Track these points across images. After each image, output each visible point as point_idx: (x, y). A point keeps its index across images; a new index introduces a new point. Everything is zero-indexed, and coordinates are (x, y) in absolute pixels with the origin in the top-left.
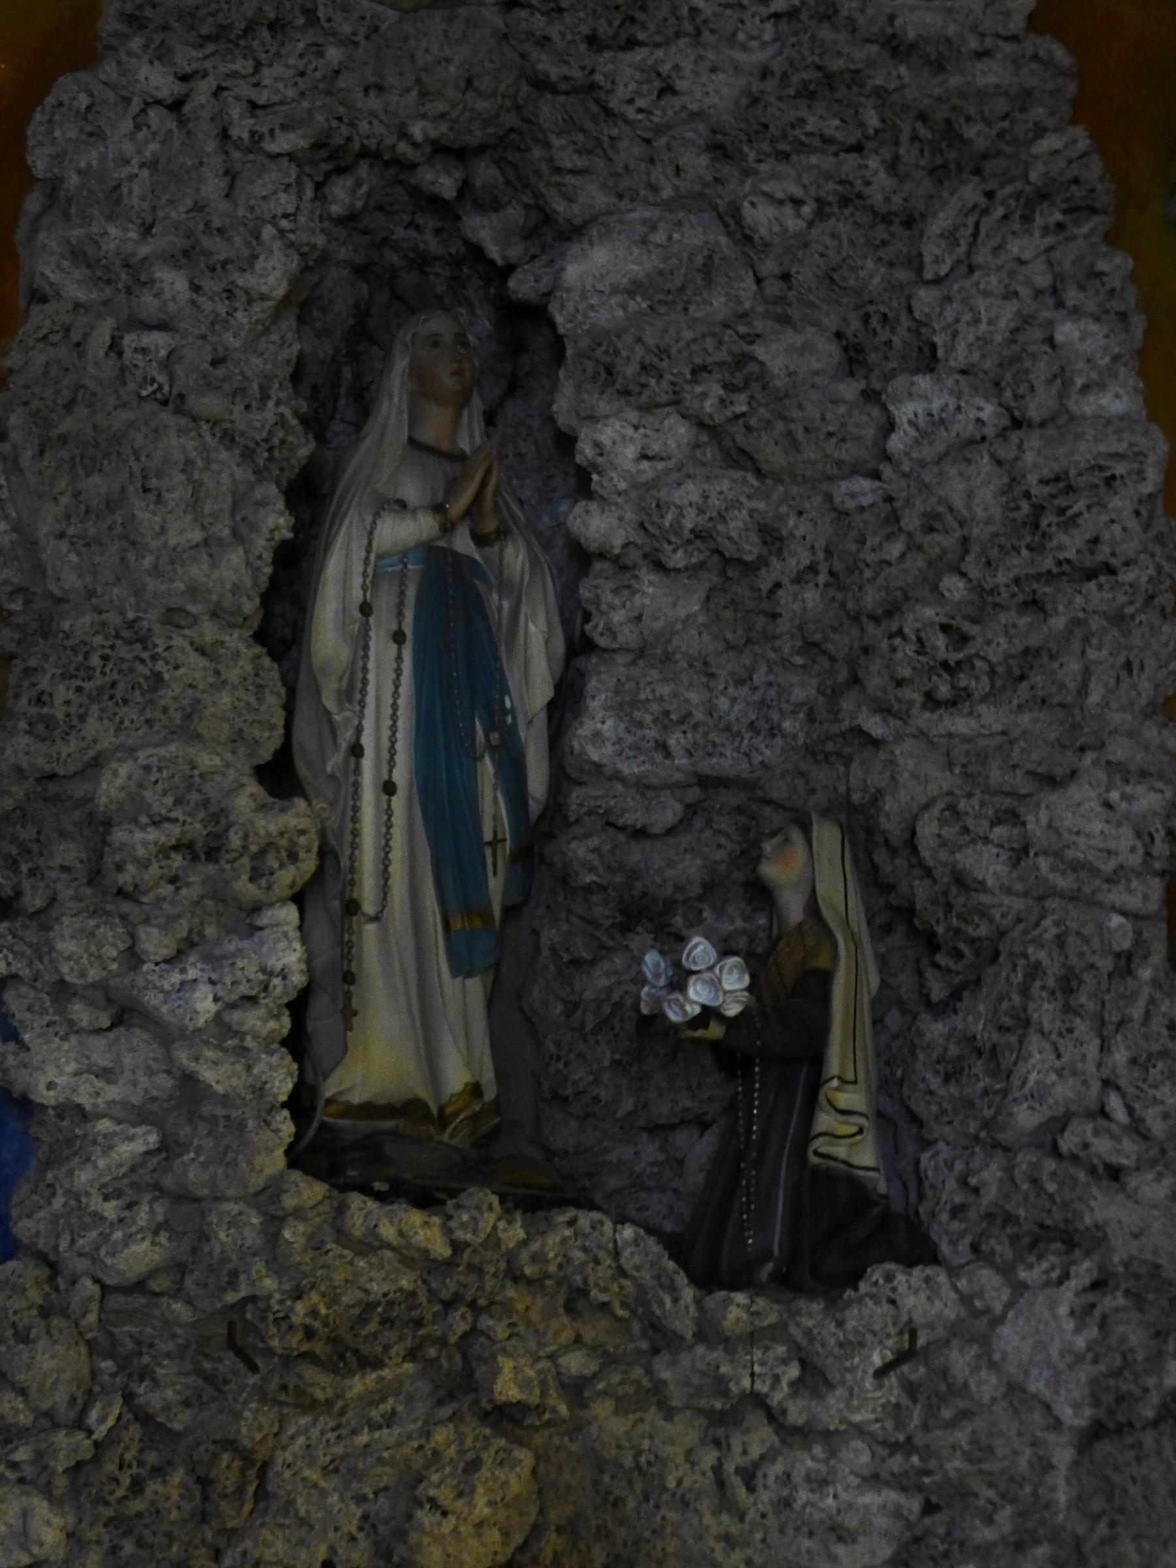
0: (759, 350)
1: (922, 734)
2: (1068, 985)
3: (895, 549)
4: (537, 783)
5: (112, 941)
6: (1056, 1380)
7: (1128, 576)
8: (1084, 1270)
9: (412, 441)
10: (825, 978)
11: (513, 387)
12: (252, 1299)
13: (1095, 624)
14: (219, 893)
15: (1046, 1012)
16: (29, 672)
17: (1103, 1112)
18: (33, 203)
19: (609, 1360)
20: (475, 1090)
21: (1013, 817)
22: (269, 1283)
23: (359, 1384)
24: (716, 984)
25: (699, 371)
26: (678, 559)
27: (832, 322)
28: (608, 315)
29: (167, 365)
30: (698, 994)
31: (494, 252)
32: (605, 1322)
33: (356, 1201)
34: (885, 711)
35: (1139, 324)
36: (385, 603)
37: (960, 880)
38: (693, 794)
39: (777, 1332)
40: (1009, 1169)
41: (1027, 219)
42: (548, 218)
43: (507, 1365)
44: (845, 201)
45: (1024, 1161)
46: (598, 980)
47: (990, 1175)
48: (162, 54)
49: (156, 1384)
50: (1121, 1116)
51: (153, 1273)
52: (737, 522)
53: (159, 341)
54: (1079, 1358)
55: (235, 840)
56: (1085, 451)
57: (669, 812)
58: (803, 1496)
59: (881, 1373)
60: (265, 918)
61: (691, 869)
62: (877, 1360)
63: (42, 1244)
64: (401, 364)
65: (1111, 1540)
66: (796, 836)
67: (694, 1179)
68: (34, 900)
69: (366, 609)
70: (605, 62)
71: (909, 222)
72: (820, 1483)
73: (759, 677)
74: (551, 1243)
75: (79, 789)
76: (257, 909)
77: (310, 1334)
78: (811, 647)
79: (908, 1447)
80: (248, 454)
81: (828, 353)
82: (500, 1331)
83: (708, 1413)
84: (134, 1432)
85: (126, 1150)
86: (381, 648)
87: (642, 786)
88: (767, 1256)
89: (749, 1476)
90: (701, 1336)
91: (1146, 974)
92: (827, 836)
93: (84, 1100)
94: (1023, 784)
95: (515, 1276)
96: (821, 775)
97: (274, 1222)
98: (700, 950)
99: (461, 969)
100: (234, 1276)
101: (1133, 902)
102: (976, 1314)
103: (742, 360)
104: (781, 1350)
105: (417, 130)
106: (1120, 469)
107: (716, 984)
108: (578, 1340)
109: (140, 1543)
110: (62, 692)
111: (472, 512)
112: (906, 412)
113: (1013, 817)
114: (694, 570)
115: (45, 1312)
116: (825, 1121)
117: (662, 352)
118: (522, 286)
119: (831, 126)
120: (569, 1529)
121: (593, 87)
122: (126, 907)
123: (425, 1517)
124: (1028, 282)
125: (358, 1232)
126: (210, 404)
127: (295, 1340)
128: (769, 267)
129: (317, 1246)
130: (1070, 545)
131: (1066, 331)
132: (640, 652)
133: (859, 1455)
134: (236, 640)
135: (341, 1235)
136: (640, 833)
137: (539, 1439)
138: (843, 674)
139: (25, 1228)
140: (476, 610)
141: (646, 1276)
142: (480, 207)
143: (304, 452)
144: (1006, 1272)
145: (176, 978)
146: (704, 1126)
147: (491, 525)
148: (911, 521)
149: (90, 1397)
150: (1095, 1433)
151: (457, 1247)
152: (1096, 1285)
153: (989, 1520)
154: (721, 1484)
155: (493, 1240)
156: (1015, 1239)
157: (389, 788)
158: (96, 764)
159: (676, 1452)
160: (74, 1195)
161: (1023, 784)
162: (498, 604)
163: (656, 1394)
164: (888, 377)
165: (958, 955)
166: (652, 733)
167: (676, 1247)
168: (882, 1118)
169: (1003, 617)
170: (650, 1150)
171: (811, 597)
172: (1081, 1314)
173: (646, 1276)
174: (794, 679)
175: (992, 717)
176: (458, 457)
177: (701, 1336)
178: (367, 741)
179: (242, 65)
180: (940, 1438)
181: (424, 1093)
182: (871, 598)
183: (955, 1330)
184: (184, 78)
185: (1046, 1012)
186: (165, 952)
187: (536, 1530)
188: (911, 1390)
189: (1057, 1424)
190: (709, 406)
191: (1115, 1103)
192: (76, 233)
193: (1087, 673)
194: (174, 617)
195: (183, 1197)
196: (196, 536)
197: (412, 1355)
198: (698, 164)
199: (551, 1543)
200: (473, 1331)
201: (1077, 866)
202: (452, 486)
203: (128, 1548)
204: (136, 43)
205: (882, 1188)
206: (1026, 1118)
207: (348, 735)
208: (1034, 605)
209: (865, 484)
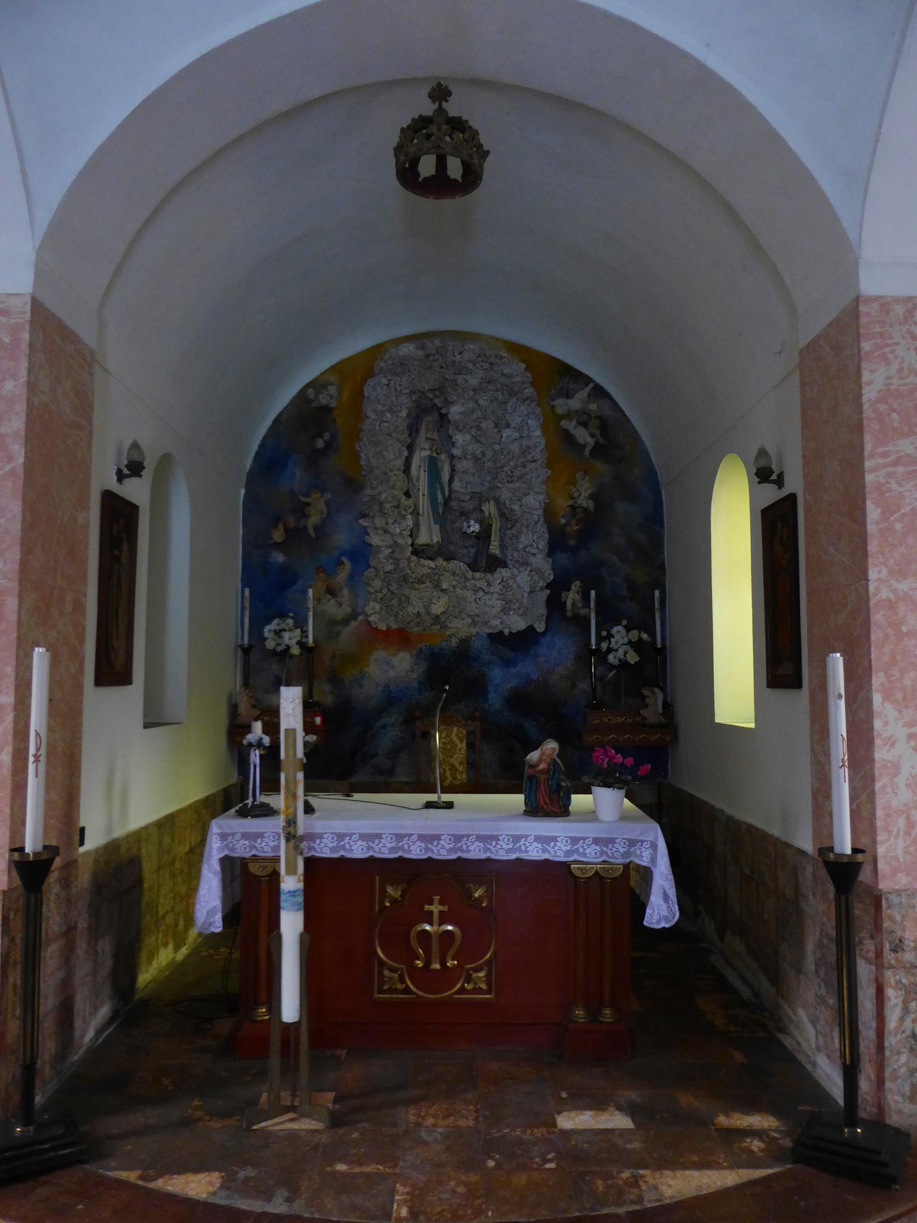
0: (481, 424)
1: (506, 487)
2: (528, 526)
3: (503, 457)
4: (447, 493)
5: (384, 521)
6: (525, 585)
7: (538, 462)
8: (529, 569)
9: (426, 438)
10: (492, 525)
11: (442, 426)
12: (406, 574)
13: (534, 469)
14: (399, 513)
15: (524, 530)
16: (369, 479)
17: (533, 546)
18: (365, 401)
19: (459, 583)
20: (438, 542)
21: (520, 500)
22: (409, 572)
23: (422, 586)
24: (474, 527)
25: (472, 427)
26: (468, 457)
27: (493, 419)
28: (458, 417)
29: (388, 428)
30: (472, 529)
31: (439, 405)
32: (458, 577)
33: (421, 559)
34: (501, 483)
35: (542, 419)
36: (422, 465)
37: (512, 510)
38: (472, 494)
39: (484, 578)
40: (519, 554)
41: (524, 403)
42: (447, 400)
43: (444, 583)
44: (495, 400)
45: (521, 552)
46: (457, 524)
47: (516, 554)
48: (385, 377)
49: (392, 586)
50: (535, 546)
51: (391, 570)
52: (478, 452)
53: (386, 425)
54: (528, 581)
55: (402, 505)
56: (531, 443)
57: (468, 498)
58: (488, 601)
59: (499, 584)
60: (406, 517)
61: (471, 507)
62: (498, 582)
63: (374, 566)
64: (424, 425)
65: (532, 608)
66: (487, 503)
67: (472, 555)
68: (371, 514)
69: (420, 466)
70: (457, 376)
71: (505, 403)
72: (490, 600)
73: (482, 476)
74: (450, 565)
75: (378, 497)
76: (405, 515)
77: (415, 579)
78: (490, 472)
79: (503, 594)
80: (401, 442)
81: (492, 425)
82: (443, 578)
83: (473, 590)
84: (389, 593)
85: (387, 552)
86: (422, 473)
87: (462, 493)
88: (482, 567)
89: (480, 599)
90: (472, 579)
91: (539, 524)
92: (492, 502)
93: (380, 545)
94: (522, 495)
95: (445, 570)
96: (491, 492)
97: (409, 563)
98: (472, 522)
99: (435, 524)
100: (404, 570)
101: (538, 513)
102: (513, 575)
103: (479, 426)
104: (484, 581)
105: (426, 388)
106: (538, 444)
107: (474, 527)
108: (454, 580)
109: (391, 609)
110: (375, 482)
111: (436, 450)
112: (505, 435)
113: (520, 500)
114: (471, 459)
115: (376, 576)
116: (491, 547)
117: (466, 424)
118: (443, 411)
119: (493, 388)
120: (453, 607)
121: (454, 380)
122: (385, 516)
123: (433, 605)
124: (524, 414)
125: (422, 564)
126: (395, 435)
127: (413, 580)
128: (483, 410)
129: (416, 566)
130: (530, 457)
131: (530, 422)
132: (463, 472)
133: (496, 596)
134: (400, 473)
135: (419, 564)
136: (463, 501)
137: (449, 594)
138: (495, 476)
139: (372, 564)
140: (436, 465)
141: (464, 570)
142: (436, 398)
143: (409, 442)
144: (518, 569)
145: (393, 527)
146: (473, 547)
147: (438, 452)
148: (505, 453)
149: (383, 588)
150: (531, 592)
151: (436, 566)
152: (531, 571)
153: (515, 605)
154: (476, 600)
155: (442, 565)
156: (519, 565)
157: (424, 495)
158: (380, 494)
159: (469, 596)
160: (379, 559)
161: (522, 495)
162: (440, 464)
163: (466, 587)
164: (502, 429)
165: (512, 521)
166: (464, 485)
167: (468, 565)
168: (501, 546)
169: (519, 469)
170: (465, 551)
171: (490, 464)
172: (529, 575)
173: (464, 570)
174: (487, 477)
175: (517, 485)
176: (433, 440)
177: (472, 579)
178: (420, 488)
179: (398, 379)
180: (508, 593)
181: (430, 542)
182: (499, 465)
183: (510, 578)
184: (389, 380)
185: (524, 530)
186: (392, 522)
187: (449, 607)
188: (503, 586)
189: (525, 591)
190: (474, 433)
191: (534, 544)
192: (373, 407)
193: (532, 477)
194: (391, 470)
195: (396, 559)
196: (394, 457)
197: (430, 582)
198: (471, 393)
199: (451, 609)
200: (439, 578)
201: (529, 508)
202: (433, 445)
203: (389, 610)
204: (381, 375)
205: (500, 556)
206: (521, 546)
207: (417, 487)
208: (524, 466)
209: (498, 446)
